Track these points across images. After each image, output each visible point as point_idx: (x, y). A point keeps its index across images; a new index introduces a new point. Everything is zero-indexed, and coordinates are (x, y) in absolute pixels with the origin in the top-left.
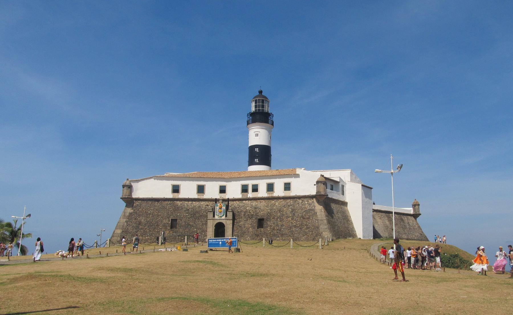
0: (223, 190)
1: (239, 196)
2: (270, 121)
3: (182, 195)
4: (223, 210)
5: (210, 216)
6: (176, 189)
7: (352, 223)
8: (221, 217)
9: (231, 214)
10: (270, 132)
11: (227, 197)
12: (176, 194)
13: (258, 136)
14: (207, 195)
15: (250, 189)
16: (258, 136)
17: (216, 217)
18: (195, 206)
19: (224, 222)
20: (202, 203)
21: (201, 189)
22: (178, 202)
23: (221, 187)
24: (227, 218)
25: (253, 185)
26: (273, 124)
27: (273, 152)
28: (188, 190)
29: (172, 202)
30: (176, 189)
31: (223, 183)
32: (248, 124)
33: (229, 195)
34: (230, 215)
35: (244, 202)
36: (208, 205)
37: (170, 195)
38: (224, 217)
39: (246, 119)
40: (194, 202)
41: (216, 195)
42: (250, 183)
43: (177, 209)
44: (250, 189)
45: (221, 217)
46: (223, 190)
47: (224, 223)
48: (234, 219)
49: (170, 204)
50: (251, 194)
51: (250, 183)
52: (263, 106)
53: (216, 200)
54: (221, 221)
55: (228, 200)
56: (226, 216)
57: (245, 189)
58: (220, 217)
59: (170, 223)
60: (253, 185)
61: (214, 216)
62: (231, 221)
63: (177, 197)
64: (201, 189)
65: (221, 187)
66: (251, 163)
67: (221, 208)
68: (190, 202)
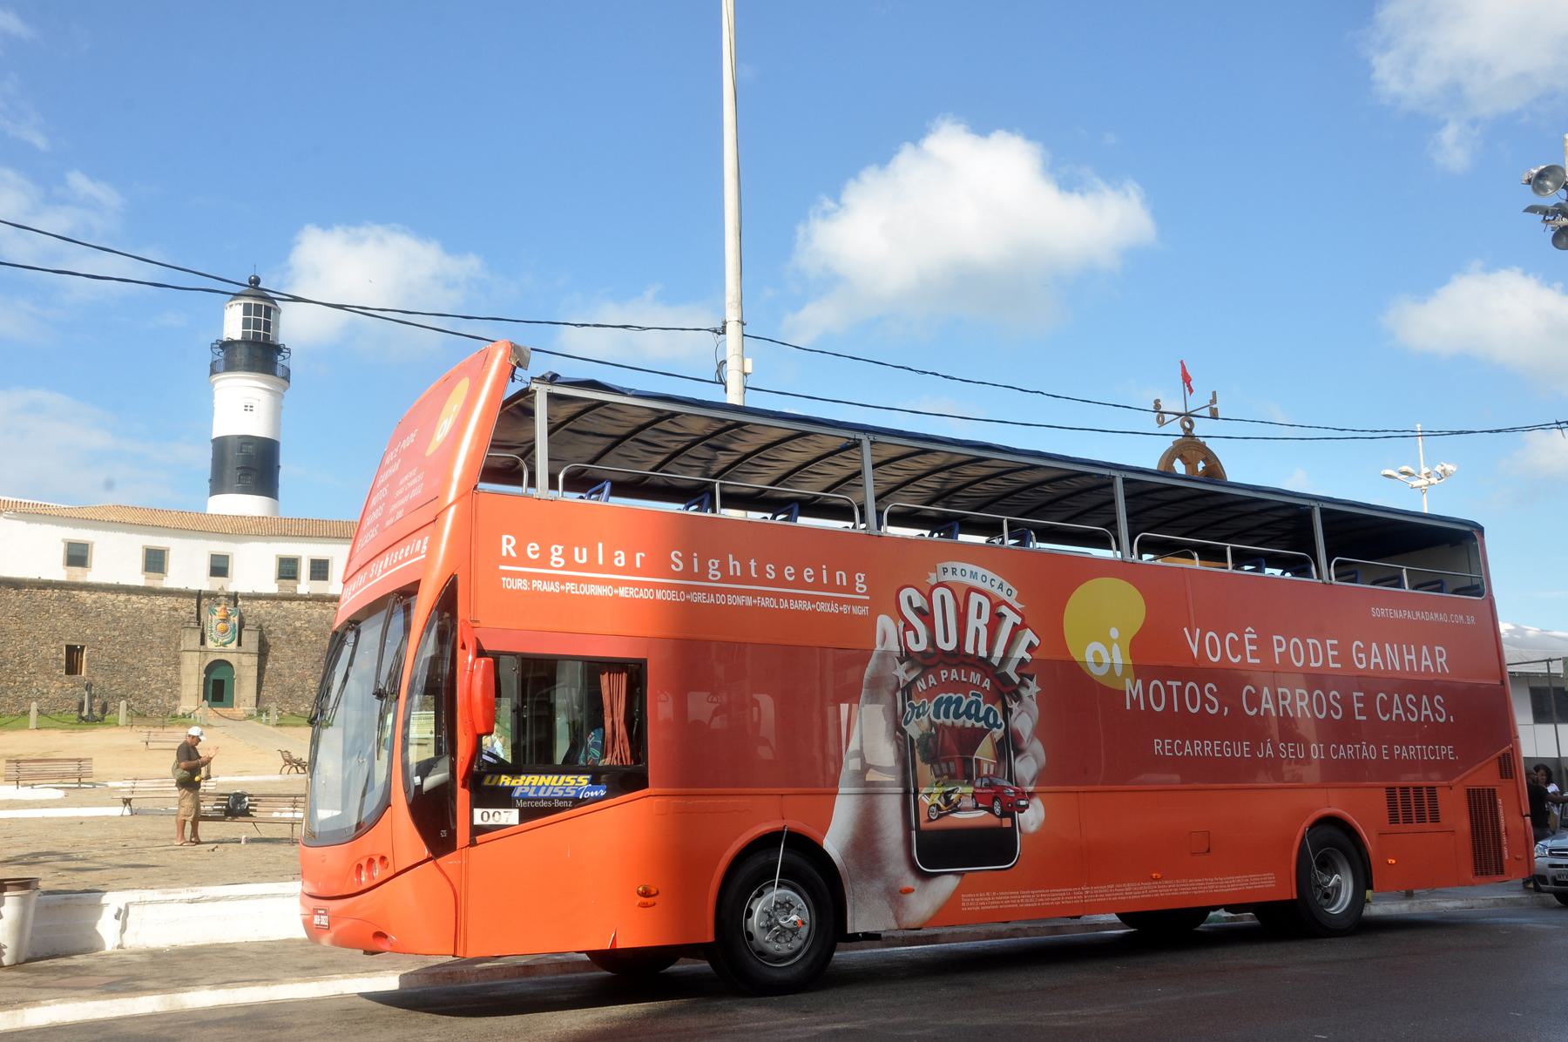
0: (219, 568)
1: (272, 587)
2: (279, 371)
3: (98, 572)
4: (230, 625)
5: (191, 640)
6: (77, 556)
7: (119, 1019)
8: (224, 645)
9: (255, 637)
10: (278, 396)
11: (231, 589)
12: (77, 570)
13: (241, 406)
14: (175, 578)
15: (305, 570)
16: (241, 406)
17: (210, 644)
18: (138, 610)
19: (232, 658)
20: (160, 601)
21: (155, 561)
22: (84, 594)
23: (214, 557)
24: (242, 649)
25: (227, 557)
26: (287, 378)
27: (283, 461)
28: (116, 561)
29: (64, 593)
30: (77, 556)
31: (220, 547)
32: (213, 372)
33: (239, 582)
34: (251, 640)
35: (286, 604)
36: (176, 610)
37: (57, 571)
38: (233, 646)
39: (208, 358)
40: (134, 598)
41: (203, 582)
42: (305, 552)
43: (81, 612)
44: (305, 570)
45: (224, 645)
46: (219, 568)
47: (234, 663)
48: (263, 652)
49: (59, 599)
50: (305, 586)
51: (305, 552)
52: (267, 326)
53: (199, 595)
54: (223, 657)
55: (234, 598)
56: (239, 644)
57: (288, 569)
58: (219, 644)
59: (63, 656)
60: (227, 557)
61: (203, 642)
62: (255, 659)
63: (80, 580)
64: (155, 561)
65: (214, 557)
66: (218, 485)
67: (225, 620)
68: (122, 597)
